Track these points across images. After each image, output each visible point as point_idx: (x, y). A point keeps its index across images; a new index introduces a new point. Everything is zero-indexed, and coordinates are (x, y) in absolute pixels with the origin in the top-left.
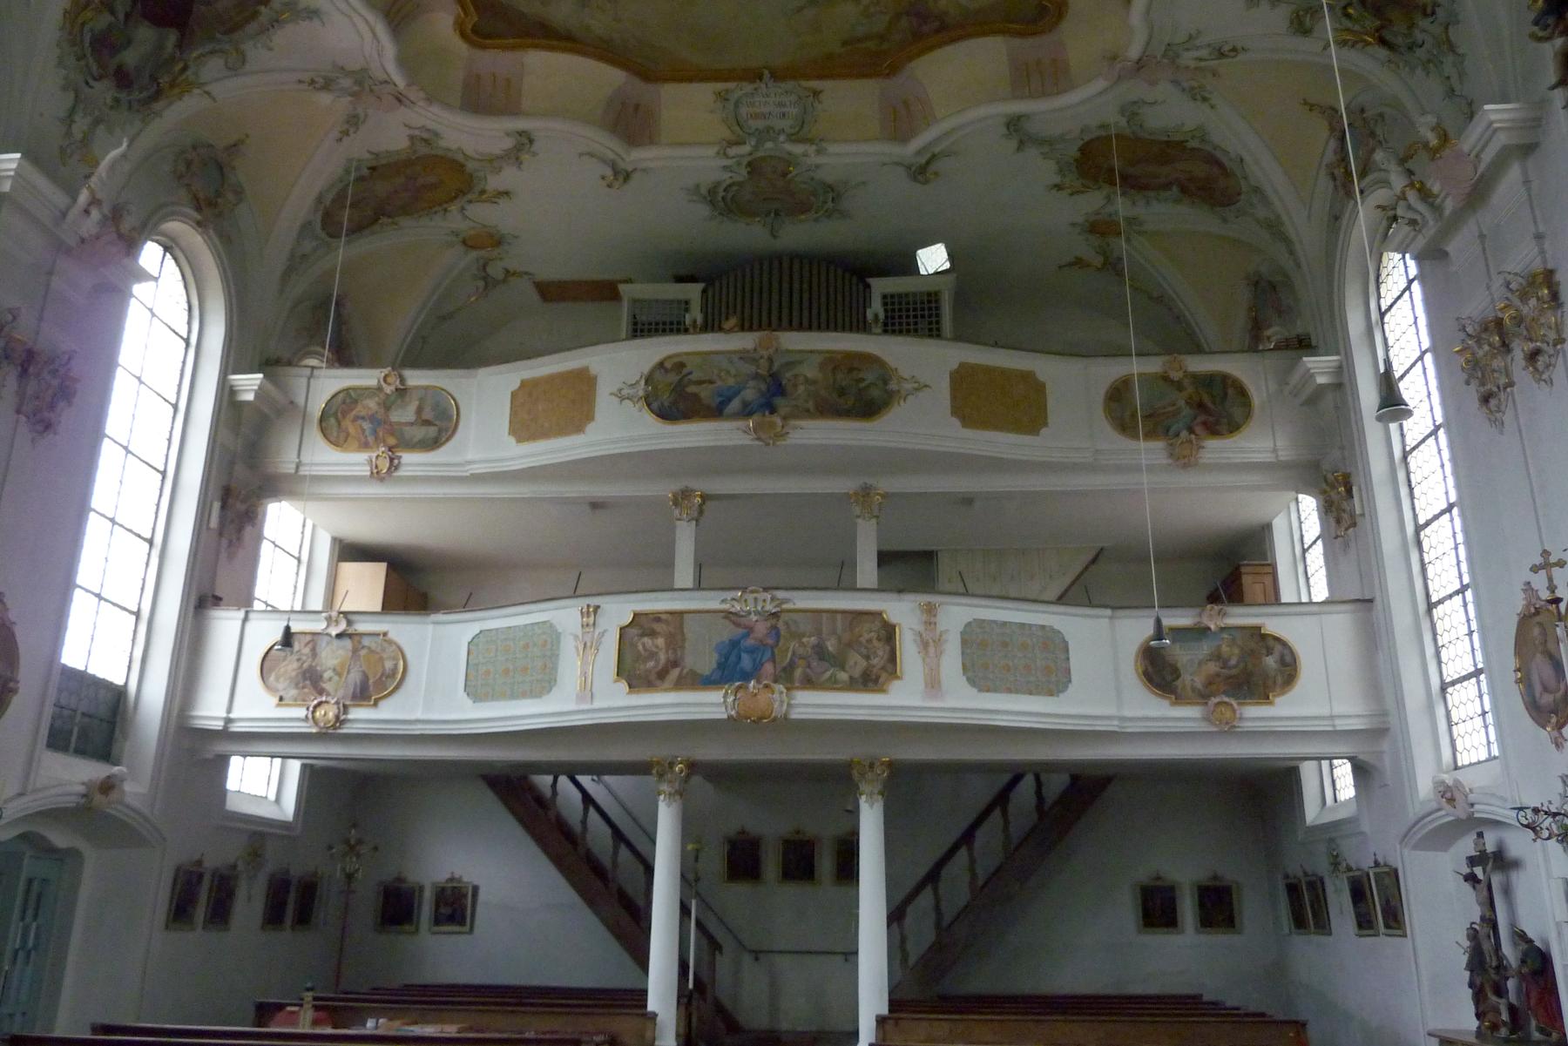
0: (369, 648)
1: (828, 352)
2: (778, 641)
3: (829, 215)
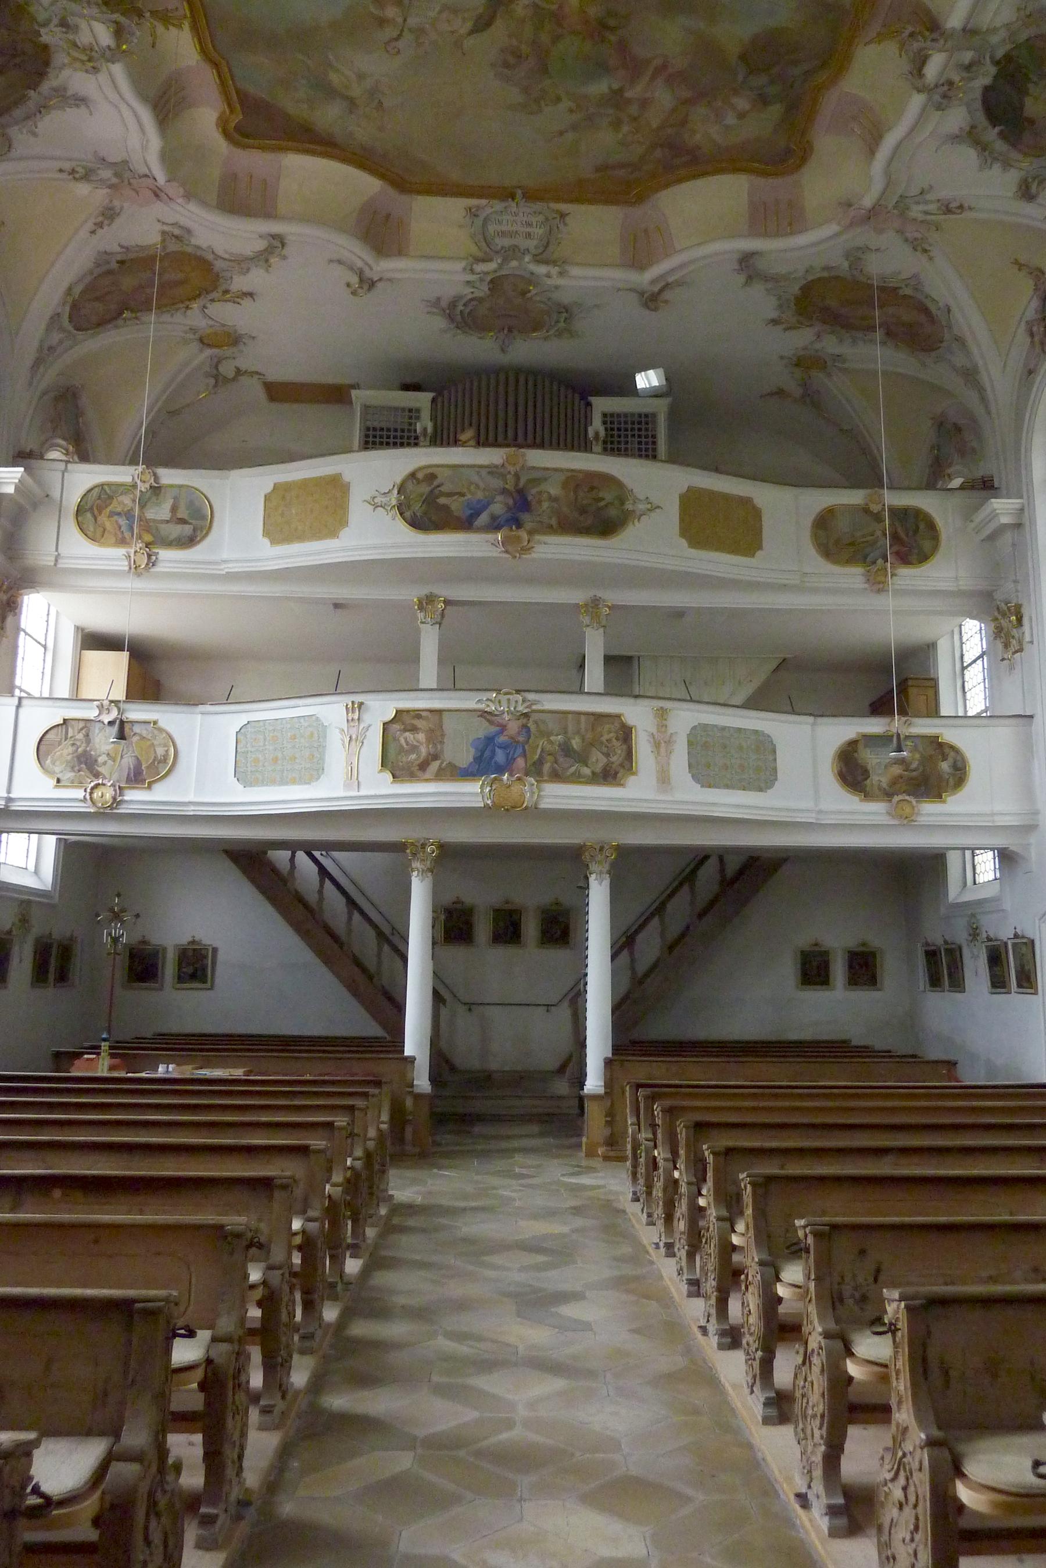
0: (140, 735)
1: (568, 470)
2: (529, 737)
3: (559, 334)
